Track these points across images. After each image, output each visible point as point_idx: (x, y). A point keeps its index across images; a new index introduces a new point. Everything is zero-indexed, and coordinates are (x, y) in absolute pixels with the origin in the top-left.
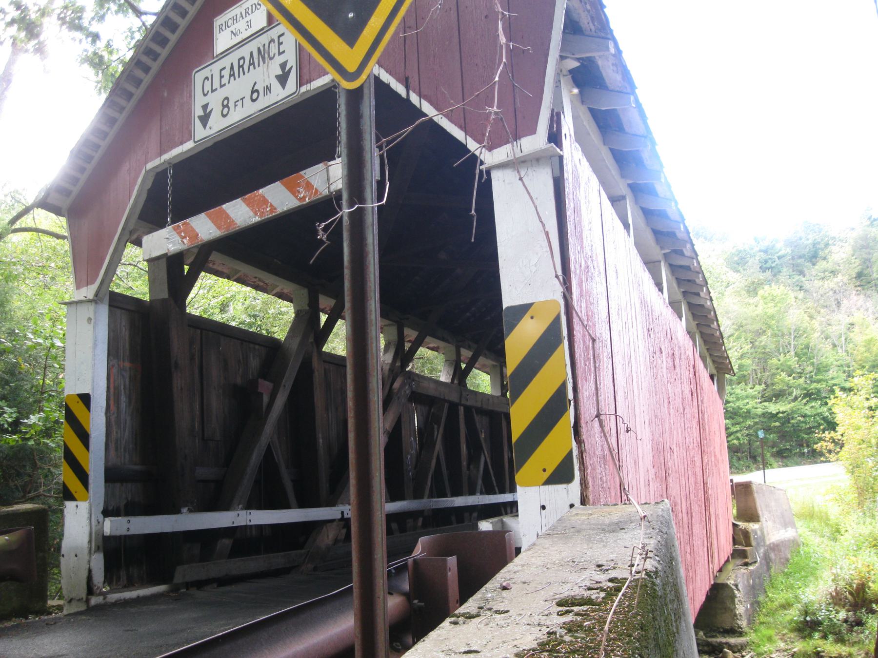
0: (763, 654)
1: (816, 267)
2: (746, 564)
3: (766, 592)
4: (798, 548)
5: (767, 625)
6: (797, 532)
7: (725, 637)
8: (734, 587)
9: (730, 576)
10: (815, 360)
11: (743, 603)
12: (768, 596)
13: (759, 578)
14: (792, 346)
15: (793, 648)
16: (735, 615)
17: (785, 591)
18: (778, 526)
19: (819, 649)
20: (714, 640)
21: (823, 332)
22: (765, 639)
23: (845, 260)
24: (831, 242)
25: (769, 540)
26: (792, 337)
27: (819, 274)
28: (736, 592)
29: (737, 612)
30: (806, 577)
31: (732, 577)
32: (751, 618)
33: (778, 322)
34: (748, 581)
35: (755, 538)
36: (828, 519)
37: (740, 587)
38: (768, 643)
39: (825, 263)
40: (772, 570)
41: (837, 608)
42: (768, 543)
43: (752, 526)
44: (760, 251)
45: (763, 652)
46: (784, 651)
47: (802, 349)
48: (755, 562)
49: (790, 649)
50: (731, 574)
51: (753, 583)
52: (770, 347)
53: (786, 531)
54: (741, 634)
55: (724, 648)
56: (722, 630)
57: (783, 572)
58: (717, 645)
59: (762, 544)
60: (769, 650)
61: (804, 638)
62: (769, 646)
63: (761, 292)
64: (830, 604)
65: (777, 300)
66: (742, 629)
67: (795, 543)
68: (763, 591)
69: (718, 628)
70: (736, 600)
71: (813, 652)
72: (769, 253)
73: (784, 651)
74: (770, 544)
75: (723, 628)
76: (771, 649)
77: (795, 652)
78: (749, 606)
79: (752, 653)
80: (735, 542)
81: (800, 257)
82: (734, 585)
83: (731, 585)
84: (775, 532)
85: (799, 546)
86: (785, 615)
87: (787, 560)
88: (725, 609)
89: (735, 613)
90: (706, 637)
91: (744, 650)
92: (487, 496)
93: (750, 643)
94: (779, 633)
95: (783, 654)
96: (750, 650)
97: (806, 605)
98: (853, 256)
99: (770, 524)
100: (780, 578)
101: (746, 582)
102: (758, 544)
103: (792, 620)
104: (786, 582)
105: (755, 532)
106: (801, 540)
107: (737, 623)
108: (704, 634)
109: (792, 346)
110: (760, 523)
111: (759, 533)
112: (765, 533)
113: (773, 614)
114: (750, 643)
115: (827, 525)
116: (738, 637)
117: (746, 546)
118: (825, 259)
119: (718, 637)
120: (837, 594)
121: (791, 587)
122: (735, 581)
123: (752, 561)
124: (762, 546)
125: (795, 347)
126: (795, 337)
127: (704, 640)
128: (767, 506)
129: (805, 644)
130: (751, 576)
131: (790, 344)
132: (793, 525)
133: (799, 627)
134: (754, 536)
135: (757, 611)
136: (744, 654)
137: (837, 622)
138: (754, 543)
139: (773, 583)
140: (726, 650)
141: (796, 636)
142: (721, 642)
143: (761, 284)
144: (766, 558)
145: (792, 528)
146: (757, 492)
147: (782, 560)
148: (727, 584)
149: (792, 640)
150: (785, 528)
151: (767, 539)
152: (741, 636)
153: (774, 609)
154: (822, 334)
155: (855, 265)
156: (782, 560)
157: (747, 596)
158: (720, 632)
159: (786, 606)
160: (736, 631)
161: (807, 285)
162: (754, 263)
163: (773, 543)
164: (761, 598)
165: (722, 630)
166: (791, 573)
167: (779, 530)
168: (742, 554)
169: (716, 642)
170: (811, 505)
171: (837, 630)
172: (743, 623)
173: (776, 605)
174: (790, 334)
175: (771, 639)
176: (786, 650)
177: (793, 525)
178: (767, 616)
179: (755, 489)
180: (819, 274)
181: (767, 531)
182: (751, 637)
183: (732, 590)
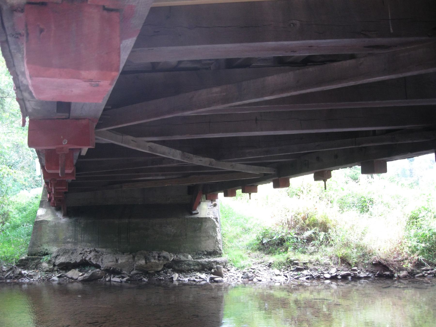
8: (215, 220)
16: (217, 241)
52: (242, 263)
61: (379, 322)
63: (162, 266)
69: (203, 252)
75: (207, 252)
82: (215, 219)
83: (212, 219)
88: (208, 237)
92: (251, 133)
158: (204, 255)
165: (206, 253)
170: (366, 246)
183: (214, 222)
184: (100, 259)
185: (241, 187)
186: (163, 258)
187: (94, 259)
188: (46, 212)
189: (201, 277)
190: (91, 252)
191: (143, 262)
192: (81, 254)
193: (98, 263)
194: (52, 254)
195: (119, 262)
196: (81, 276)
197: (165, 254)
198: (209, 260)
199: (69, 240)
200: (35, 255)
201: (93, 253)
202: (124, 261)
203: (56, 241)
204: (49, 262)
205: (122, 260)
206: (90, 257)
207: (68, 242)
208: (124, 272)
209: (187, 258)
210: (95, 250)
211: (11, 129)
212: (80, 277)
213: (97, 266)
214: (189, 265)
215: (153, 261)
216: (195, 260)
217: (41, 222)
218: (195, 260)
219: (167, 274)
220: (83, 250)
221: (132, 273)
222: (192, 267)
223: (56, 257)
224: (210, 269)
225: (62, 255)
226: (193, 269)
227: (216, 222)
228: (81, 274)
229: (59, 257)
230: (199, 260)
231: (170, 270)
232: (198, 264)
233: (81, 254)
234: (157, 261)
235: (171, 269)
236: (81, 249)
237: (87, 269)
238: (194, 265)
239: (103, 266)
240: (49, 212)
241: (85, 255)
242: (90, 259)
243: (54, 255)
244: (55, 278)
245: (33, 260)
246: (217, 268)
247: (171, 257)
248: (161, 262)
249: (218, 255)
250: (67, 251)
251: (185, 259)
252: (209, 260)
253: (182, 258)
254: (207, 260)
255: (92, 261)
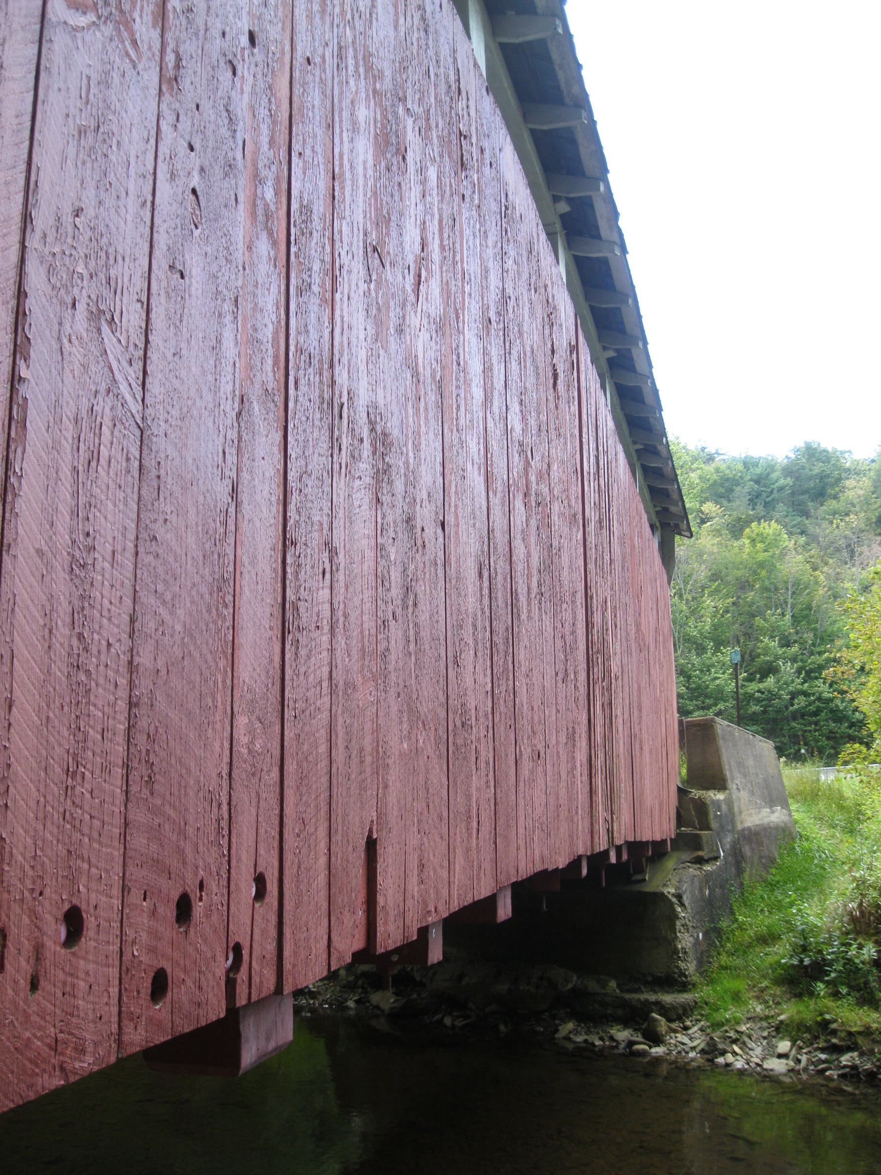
0: (723, 1025)
1: (824, 508)
2: (700, 861)
3: (732, 913)
4: (791, 842)
5: (734, 972)
6: (790, 815)
7: (655, 992)
8: (674, 900)
9: (670, 880)
10: (818, 625)
11: (691, 929)
12: (737, 920)
13: (722, 887)
14: (789, 606)
15: (779, 1015)
16: (676, 951)
17: (767, 914)
18: (758, 801)
19: (827, 1017)
20: (636, 996)
21: (830, 589)
22: (728, 999)
23: (862, 498)
24: (843, 475)
25: (742, 823)
26: (790, 593)
27: (827, 517)
28: (679, 909)
29: (680, 946)
30: (806, 889)
31: (673, 882)
32: (705, 959)
33: (770, 572)
34: (701, 890)
35: (716, 816)
36: (842, 797)
37: (686, 900)
38: (733, 1004)
39: (834, 502)
40: (746, 875)
41: (860, 940)
42: (739, 827)
43: (712, 795)
44: (751, 480)
45: (723, 1020)
46: (761, 1019)
47: (802, 610)
48: (716, 858)
49: (772, 1017)
50: (670, 876)
51: (709, 894)
53: (773, 812)
54: (684, 987)
55: (652, 1012)
56: (650, 979)
57: (765, 881)
58: (639, 1006)
59: (730, 828)
60: (735, 1018)
61: (799, 996)
62: (734, 1009)
64: (847, 934)
65: (768, 541)
66: (686, 977)
67: (787, 832)
68: (727, 911)
70: (678, 923)
71: (817, 1023)
72: (762, 484)
73: (761, 1019)
74: (743, 830)
76: (738, 1015)
77: (781, 1022)
78: (701, 935)
79: (702, 1023)
80: (680, 820)
81: (804, 492)
83: (670, 896)
84: (753, 811)
85: (793, 839)
86: (766, 954)
87: (772, 861)
89: (676, 948)
90: (621, 991)
91: (688, 1018)
93: (700, 1004)
94: (754, 986)
95: (759, 1025)
96: (699, 1017)
97: (804, 935)
98: (873, 493)
99: (744, 795)
100: (759, 891)
101: (697, 892)
102: (722, 827)
103: (778, 963)
104: (769, 898)
105: (717, 804)
106: (797, 829)
107: (678, 967)
108: (618, 986)
109: (789, 606)
110: (727, 791)
111: (724, 807)
112: (736, 809)
113: (745, 952)
114: (700, 1004)
115: (841, 808)
116: (680, 992)
117: (701, 830)
118: (835, 497)
119: (643, 992)
120: (861, 912)
121: (779, 906)
122: (677, 888)
123: (711, 855)
124: (729, 831)
125: (793, 606)
126: (794, 593)
127: (617, 997)
128: (741, 765)
129: (802, 1008)
130: (707, 882)
131: (786, 603)
132: (785, 805)
133: (789, 974)
134: (715, 812)
135: (716, 947)
136: (688, 1023)
137: (861, 966)
138: (714, 825)
139: (747, 897)
140: (654, 1015)
141: (785, 992)
142: (647, 1000)
143: (748, 522)
144: (735, 853)
145: (782, 808)
146: (724, 739)
147: (764, 860)
148: (663, 894)
149: (778, 999)
150: (771, 807)
151: (738, 819)
152: (685, 991)
153: (746, 943)
154: (828, 590)
155: (876, 506)
156: (764, 860)
157: (697, 917)
158: (646, 983)
159: (768, 939)
160: (676, 980)
161: (811, 529)
162: (742, 492)
163: (749, 829)
164: (724, 924)
165: (650, 979)
166: (778, 882)
167: (760, 808)
168: (695, 843)
169: (639, 999)
171: (862, 981)
172: (690, 967)
173: (750, 937)
174: (787, 589)
175: (739, 998)
176: (767, 1018)
177: (785, 805)
178: (733, 955)
179: (719, 731)
180: (827, 517)
181: (739, 807)
182: (704, 993)
183: (672, 904)
189: (615, 1037)
209: (604, 986)
211: (304, 657)
222: (609, 1011)
227: (676, 906)
232: (624, 1004)
235: (568, 1010)
244: (351, 1004)
249: (676, 987)
253: (592, 985)
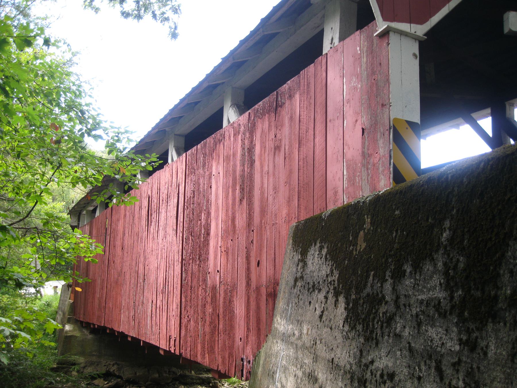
63: (171, 379)
69: (203, 369)
75: (207, 369)
158: (204, 371)
184: (122, 371)
185: (489, 111)
186: (172, 373)
187: (117, 371)
188: (74, 328)
190: (113, 365)
191: (157, 375)
192: (105, 366)
193: (120, 375)
194: (80, 364)
195: (138, 374)
196: (106, 384)
197: (174, 369)
198: (208, 376)
199: (94, 353)
200: (64, 364)
201: (116, 366)
202: (141, 374)
203: (82, 354)
204: (78, 371)
205: (140, 373)
206: (113, 369)
207: (93, 355)
208: (141, 382)
210: (116, 363)
212: (106, 385)
213: (119, 377)
214: (192, 379)
215: (164, 375)
216: (197, 375)
217: (71, 336)
218: (197, 375)
219: (174, 385)
220: (106, 362)
221: (147, 383)
223: (84, 367)
224: (209, 383)
225: (89, 366)
226: (195, 383)
228: (106, 383)
229: (87, 368)
230: (201, 376)
231: (177, 382)
233: (105, 366)
234: (168, 375)
236: (105, 362)
237: (110, 378)
238: (196, 380)
239: (125, 378)
240: (76, 328)
241: (109, 367)
242: (114, 371)
243: (82, 365)
245: (63, 368)
246: (215, 383)
247: (179, 372)
248: (171, 376)
250: (93, 363)
251: (190, 374)
252: (208, 376)
253: (187, 373)
254: (206, 376)
255: (116, 373)
